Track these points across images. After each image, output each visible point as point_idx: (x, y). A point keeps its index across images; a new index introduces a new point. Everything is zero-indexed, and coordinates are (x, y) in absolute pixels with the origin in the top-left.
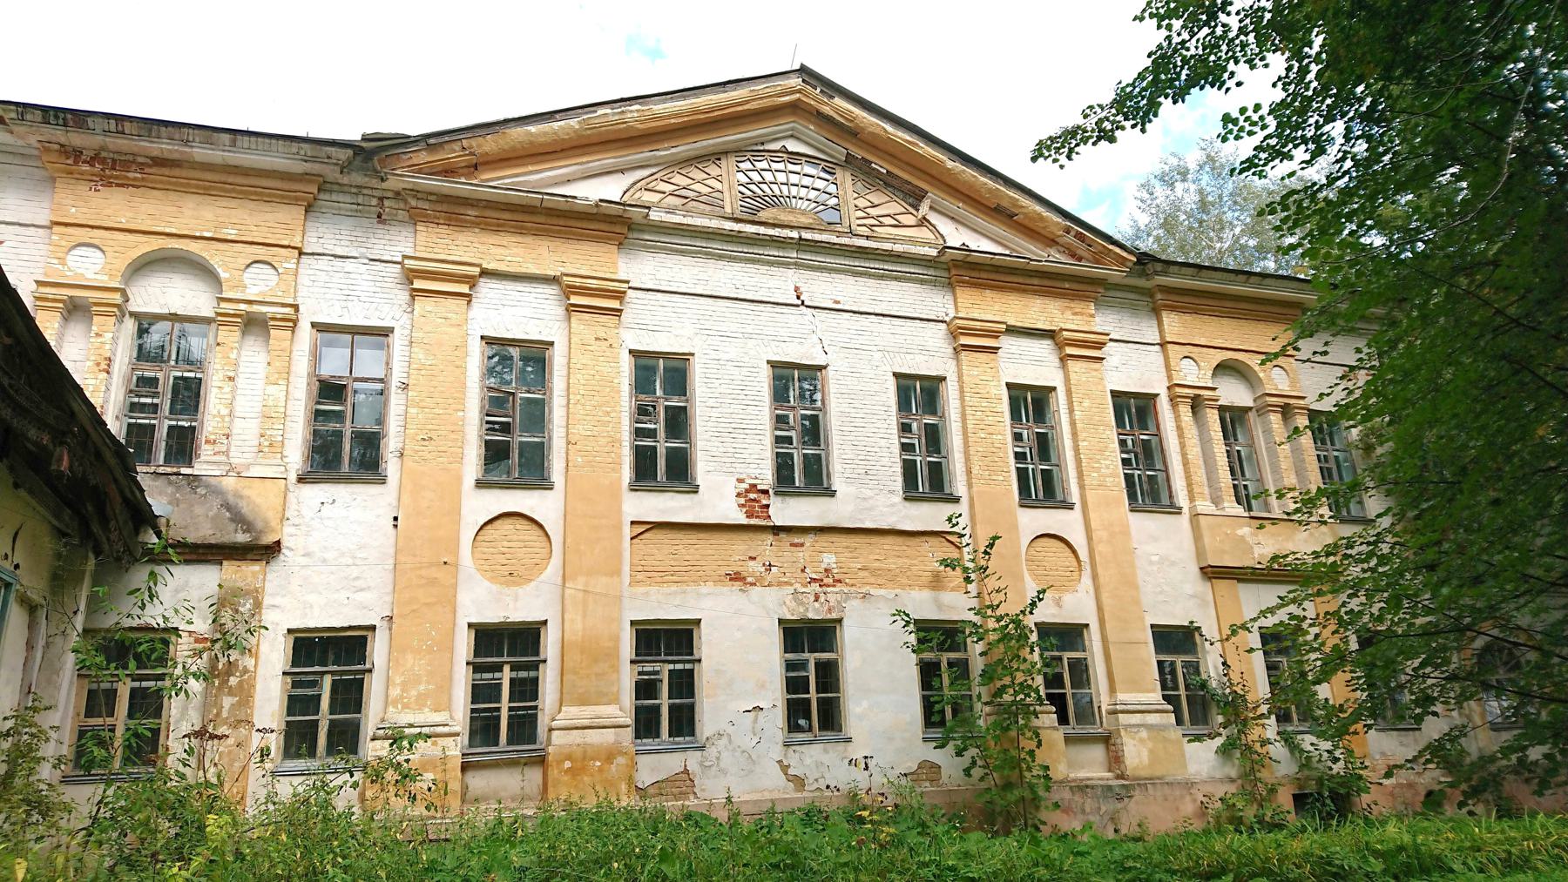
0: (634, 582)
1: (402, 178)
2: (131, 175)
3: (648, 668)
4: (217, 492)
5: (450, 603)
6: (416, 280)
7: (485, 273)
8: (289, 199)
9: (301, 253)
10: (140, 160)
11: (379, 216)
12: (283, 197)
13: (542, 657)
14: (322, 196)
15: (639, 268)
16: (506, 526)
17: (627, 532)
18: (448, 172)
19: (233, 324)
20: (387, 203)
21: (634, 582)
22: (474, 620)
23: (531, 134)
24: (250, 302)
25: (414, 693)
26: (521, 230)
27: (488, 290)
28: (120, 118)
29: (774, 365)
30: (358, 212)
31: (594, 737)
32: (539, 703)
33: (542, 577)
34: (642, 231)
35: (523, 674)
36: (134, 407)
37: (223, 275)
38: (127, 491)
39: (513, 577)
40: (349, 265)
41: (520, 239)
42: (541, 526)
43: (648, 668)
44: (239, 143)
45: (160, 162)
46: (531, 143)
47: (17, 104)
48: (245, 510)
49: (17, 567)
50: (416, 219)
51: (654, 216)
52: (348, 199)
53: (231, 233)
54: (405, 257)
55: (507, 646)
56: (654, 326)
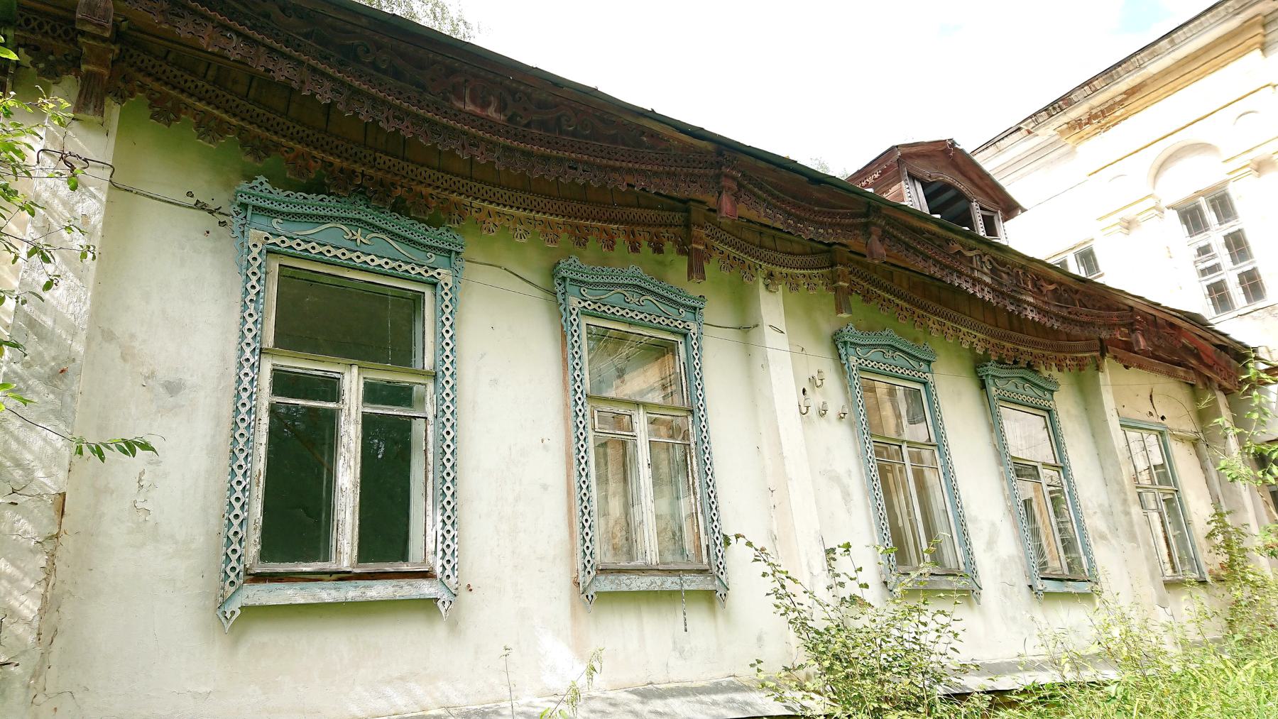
2: (1117, 114)
10: (1118, 99)
29: (1209, 245)
36: (1204, 272)
38: (1214, 340)
44: (1177, 41)
45: (1131, 92)
49: (1163, 418)
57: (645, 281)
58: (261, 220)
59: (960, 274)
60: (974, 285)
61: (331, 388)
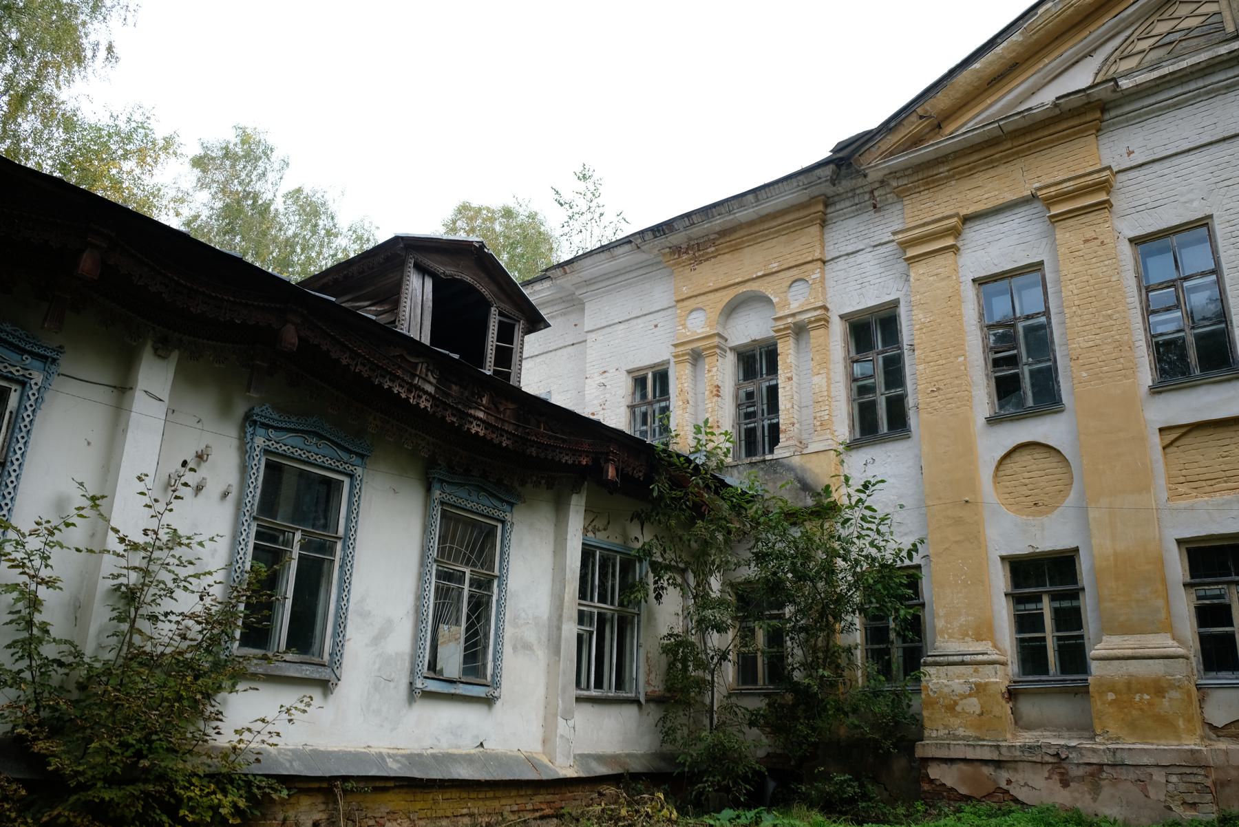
0: (1174, 495)
1: (875, 165)
3: (1214, 590)
4: (790, 469)
5: (974, 538)
6: (912, 249)
7: (966, 219)
8: (803, 225)
9: (824, 262)
11: (875, 207)
12: (802, 223)
13: (1080, 586)
14: (829, 210)
15: (1115, 149)
16: (1024, 459)
17: (1156, 441)
18: (916, 141)
19: (787, 336)
20: (876, 193)
21: (1174, 495)
22: (1004, 553)
23: (977, 71)
24: (793, 315)
25: (956, 624)
26: (991, 164)
27: (976, 235)
28: (688, 215)
30: (859, 210)
31: (1135, 668)
32: (1084, 631)
33: (1066, 503)
34: (1120, 106)
35: (1066, 604)
37: (775, 300)
39: (1038, 506)
40: (860, 258)
41: (992, 173)
42: (1059, 452)
43: (1214, 590)
45: (723, 233)
46: (980, 79)
47: (638, 233)
48: (809, 481)
50: (901, 194)
51: (1125, 83)
52: (848, 203)
53: (774, 266)
54: (894, 233)
55: (1044, 577)
56: (1150, 203)
57: (274, 420)
58: (261, 431)
59: (394, 378)
60: (410, 391)
61: (460, 578)
